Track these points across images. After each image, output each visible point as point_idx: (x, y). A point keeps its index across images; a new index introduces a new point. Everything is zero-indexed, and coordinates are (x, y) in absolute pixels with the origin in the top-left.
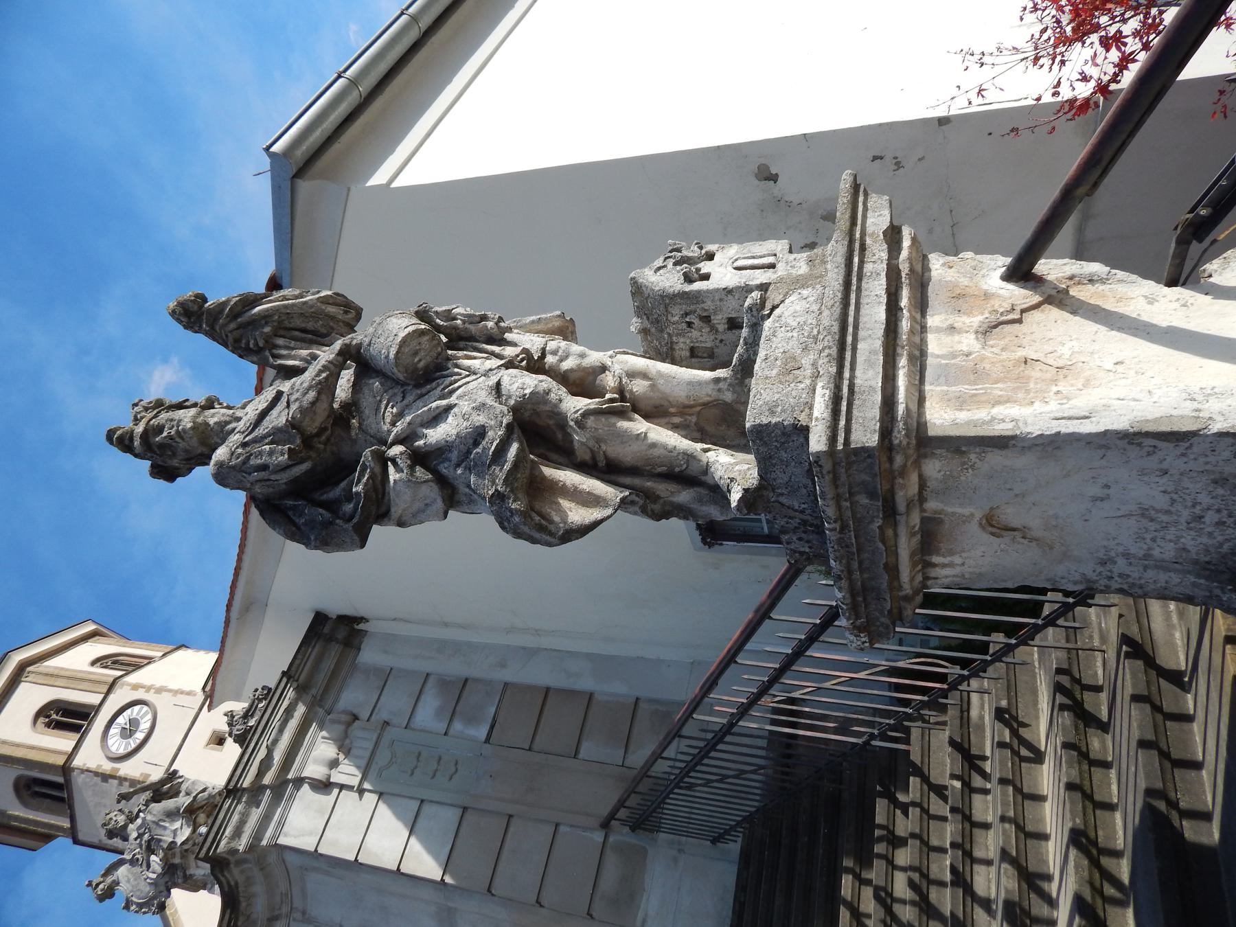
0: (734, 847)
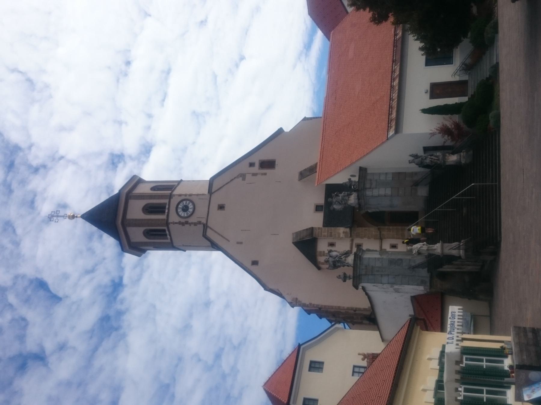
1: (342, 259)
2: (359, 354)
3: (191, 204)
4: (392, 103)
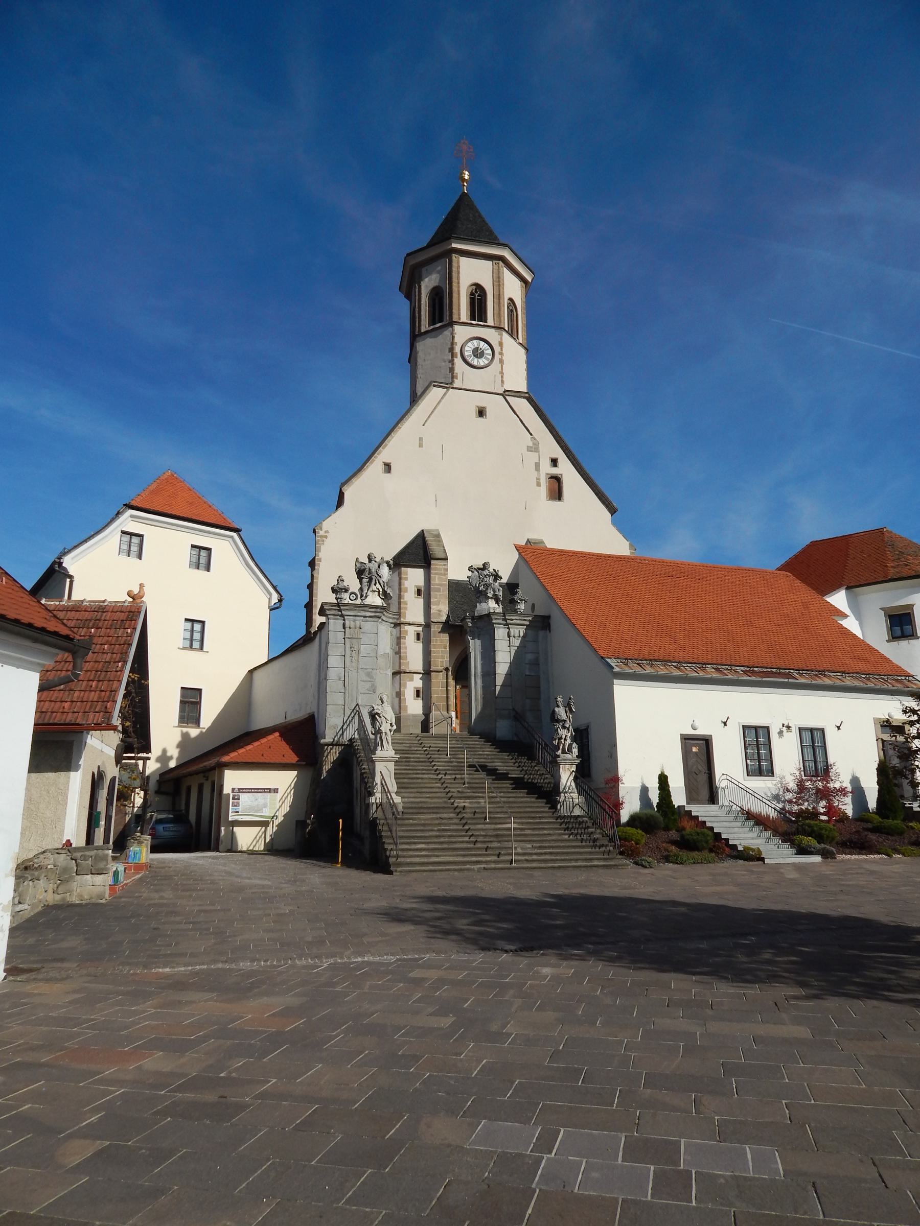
0: (515, 739)
1: (375, 585)
2: (141, 586)
3: (487, 362)
4: (688, 666)
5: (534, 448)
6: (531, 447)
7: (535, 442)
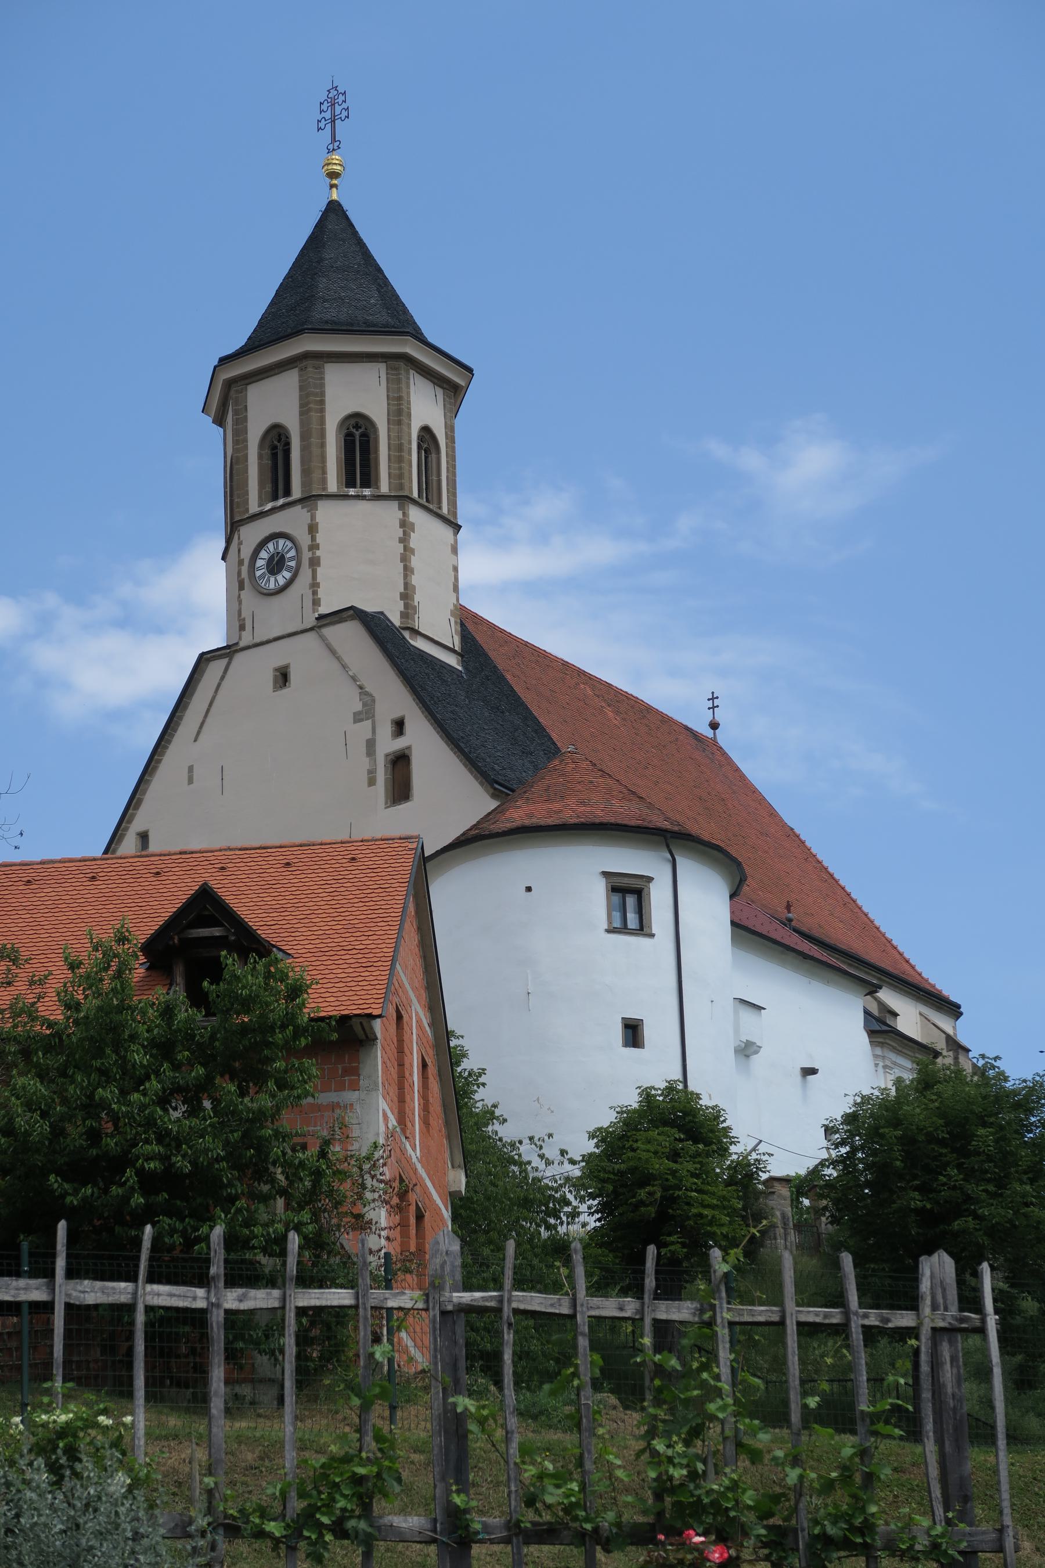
5: (366, 713)
6: (360, 713)
7: (367, 699)
